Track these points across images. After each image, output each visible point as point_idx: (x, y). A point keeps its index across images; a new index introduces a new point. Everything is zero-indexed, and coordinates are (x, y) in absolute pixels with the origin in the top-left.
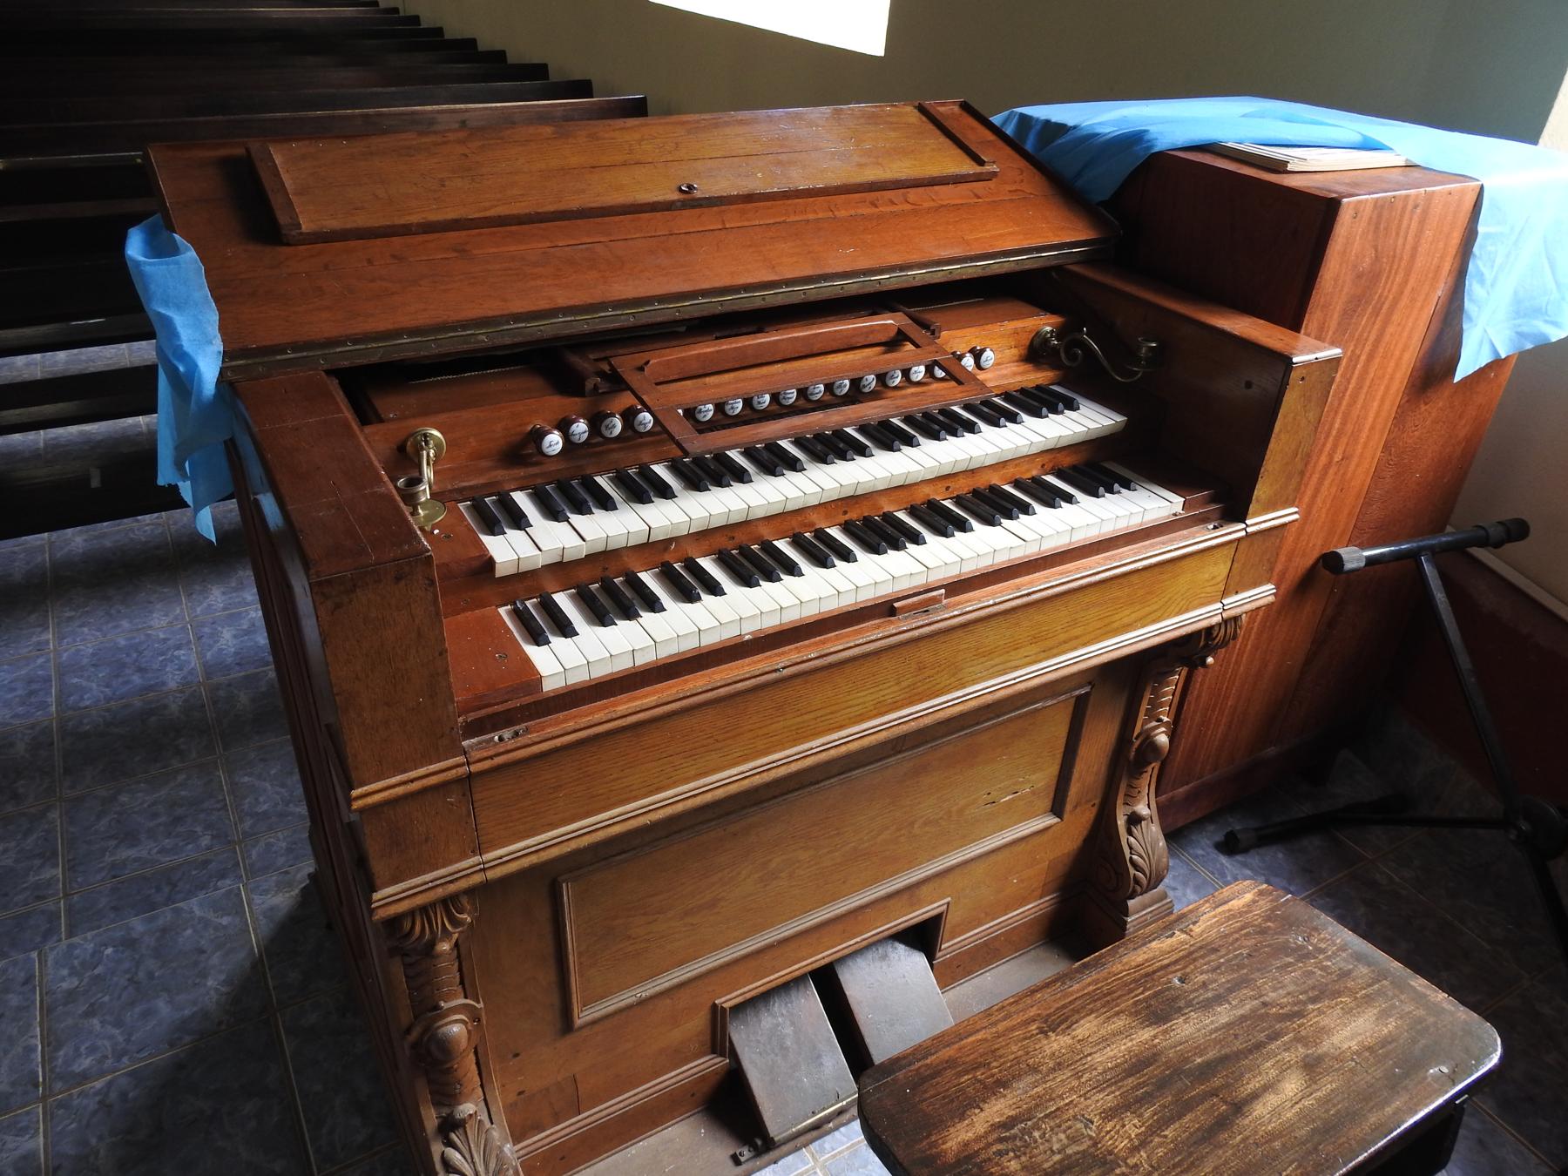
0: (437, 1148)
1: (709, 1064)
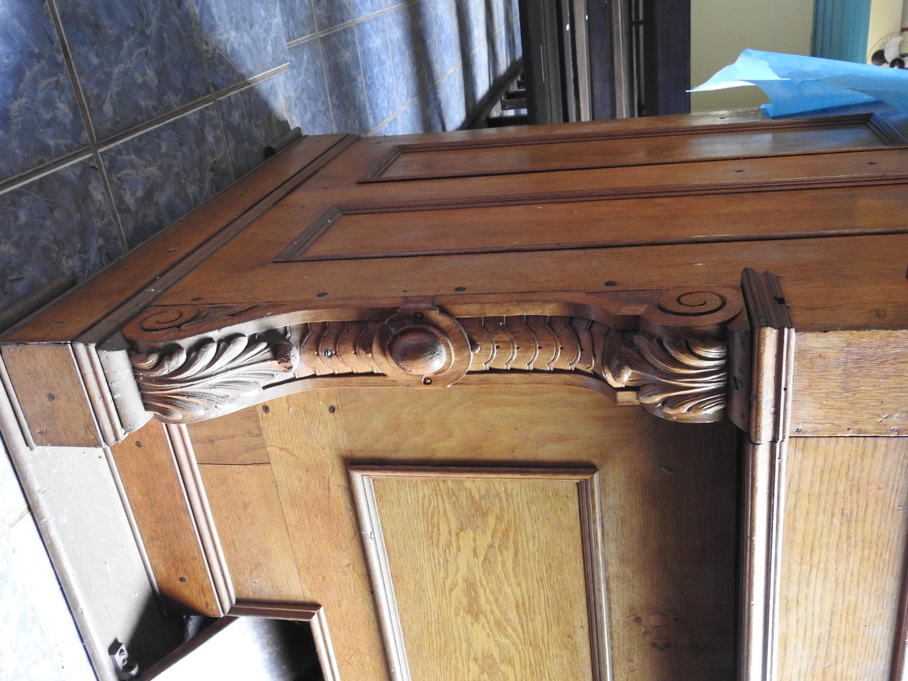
0: (249, 328)
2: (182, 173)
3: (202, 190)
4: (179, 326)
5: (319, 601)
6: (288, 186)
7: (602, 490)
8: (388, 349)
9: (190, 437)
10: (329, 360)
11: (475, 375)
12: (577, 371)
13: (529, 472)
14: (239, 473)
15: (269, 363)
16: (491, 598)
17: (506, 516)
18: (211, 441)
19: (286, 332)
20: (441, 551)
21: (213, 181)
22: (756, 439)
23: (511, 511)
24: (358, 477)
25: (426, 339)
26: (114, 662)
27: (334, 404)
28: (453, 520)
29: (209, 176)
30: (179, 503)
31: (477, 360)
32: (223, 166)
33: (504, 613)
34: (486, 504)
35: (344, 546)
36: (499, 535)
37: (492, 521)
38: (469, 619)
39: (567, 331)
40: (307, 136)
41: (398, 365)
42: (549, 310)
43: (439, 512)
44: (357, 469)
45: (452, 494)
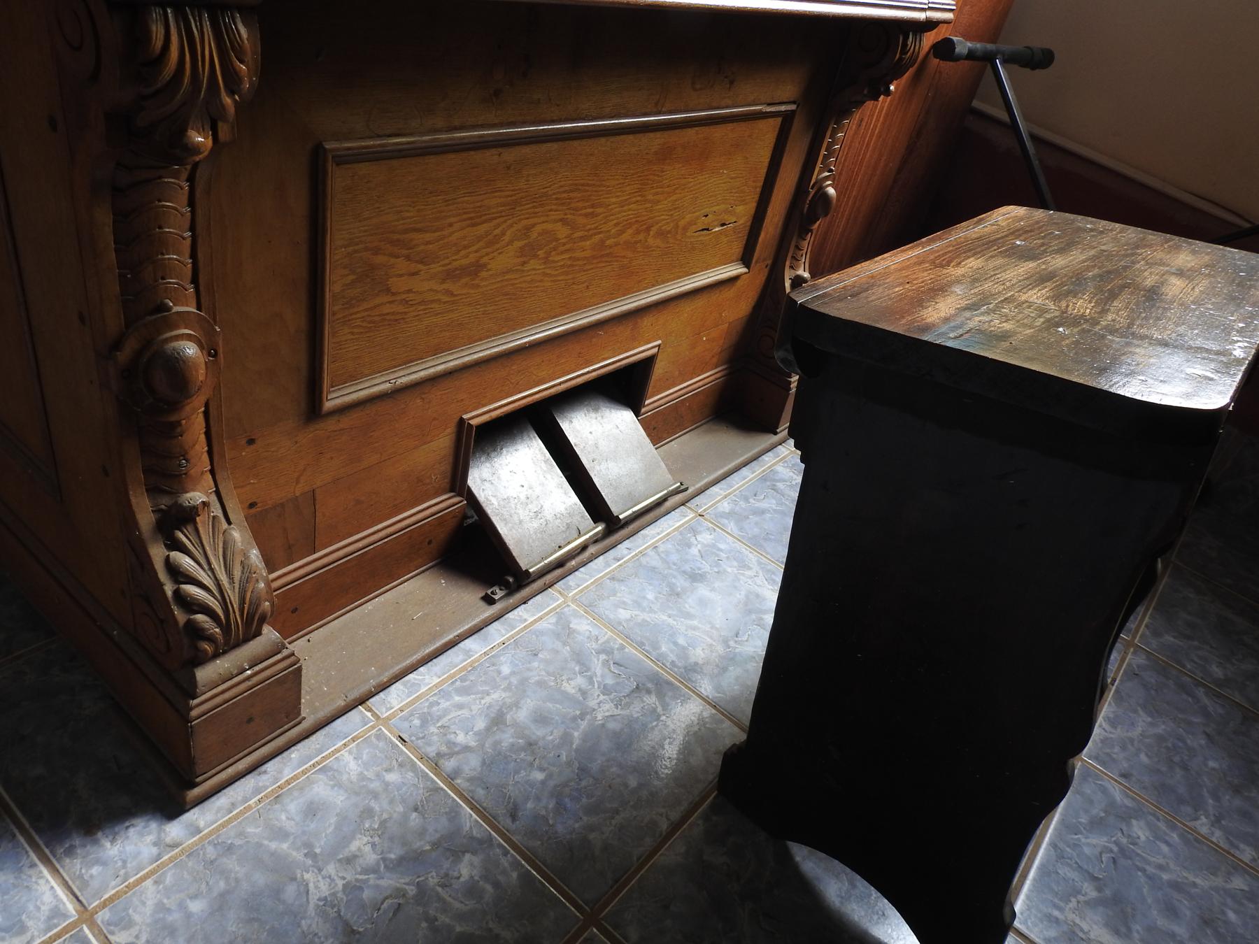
0: (158, 553)
1: (444, 503)
4: (162, 621)
5: (456, 420)
8: (175, 405)
11: (203, 300)
16: (463, 253)
18: (290, 547)
19: (161, 510)
26: (501, 598)
27: (244, 442)
28: (378, 301)
33: (479, 239)
37: (380, 259)
38: (484, 274)
42: (104, 219)
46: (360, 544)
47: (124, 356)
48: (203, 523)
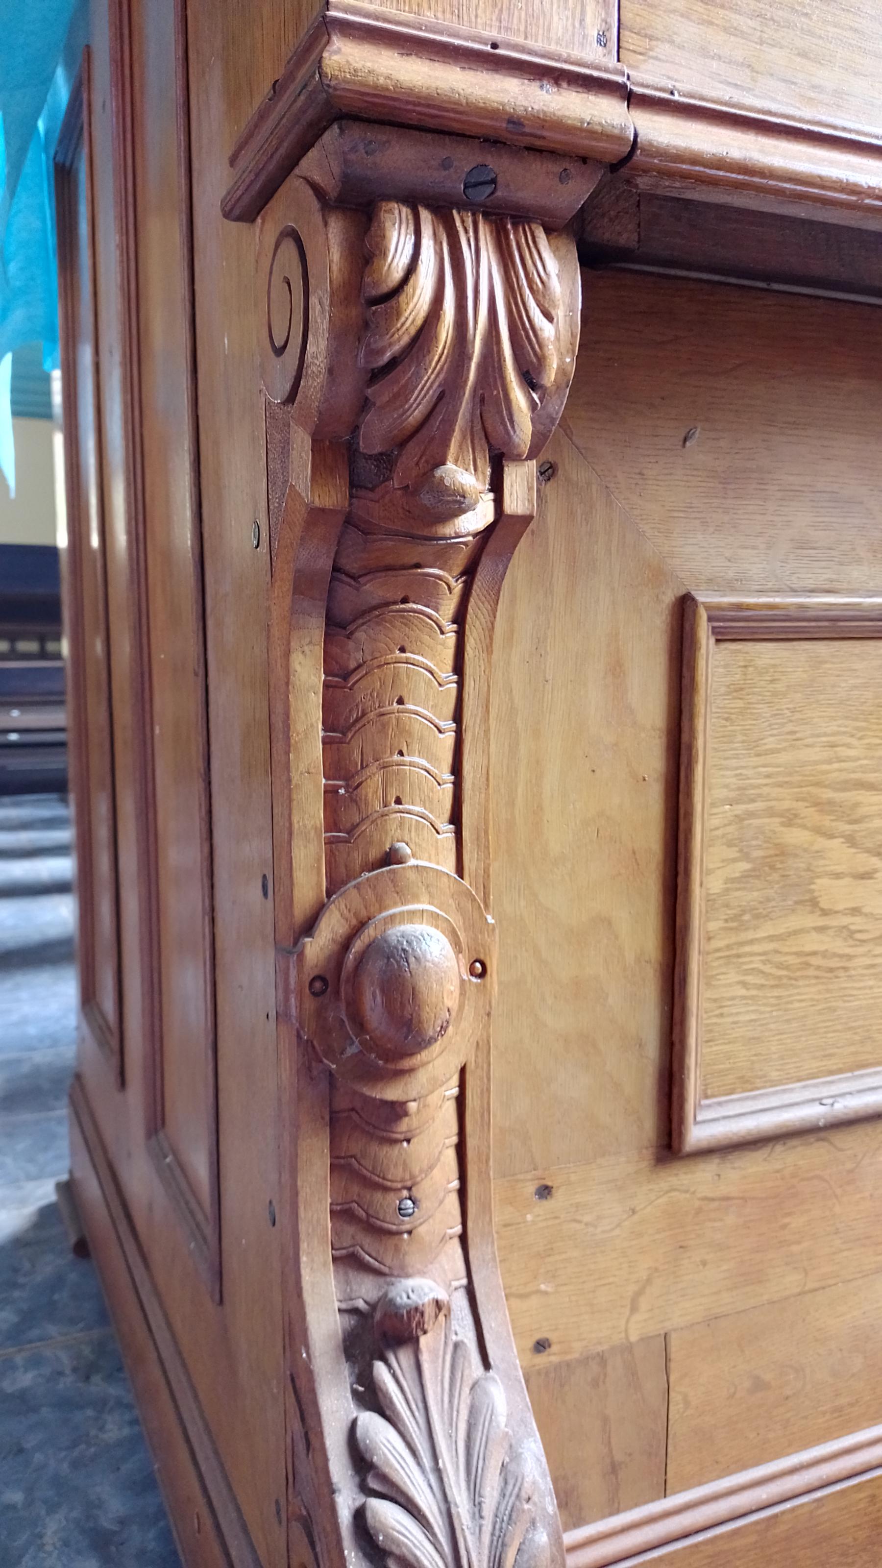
0: (336, 1406)
2: (76, 1453)
3: (120, 1404)
6: (123, 1227)
7: (731, 587)
9: (603, 1517)
10: (425, 1204)
12: (460, 619)
13: (690, 747)
14: (687, 1403)
15: (425, 1358)
17: (786, 804)
18: (614, 1468)
19: (354, 1311)
20: (861, 950)
21: (109, 1378)
22: (619, 139)
23: (775, 792)
24: (699, 1132)
25: (375, 967)
29: (98, 1386)
30: (753, 1538)
31: (428, 851)
32: (87, 1351)
34: (759, 847)
35: (849, 1166)
36: (827, 821)
39: (360, 635)
40: (71, 1172)
41: (431, 1041)
42: (308, 674)
43: (777, 952)
44: (681, 1135)
45: (737, 921)
46: (763, 1494)
47: (317, 948)
48: (434, 1352)
